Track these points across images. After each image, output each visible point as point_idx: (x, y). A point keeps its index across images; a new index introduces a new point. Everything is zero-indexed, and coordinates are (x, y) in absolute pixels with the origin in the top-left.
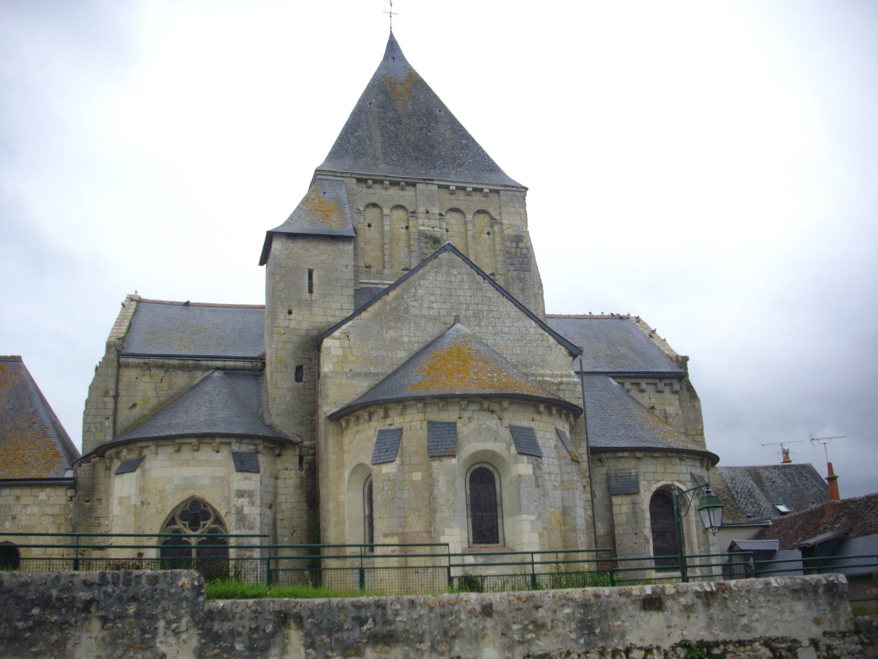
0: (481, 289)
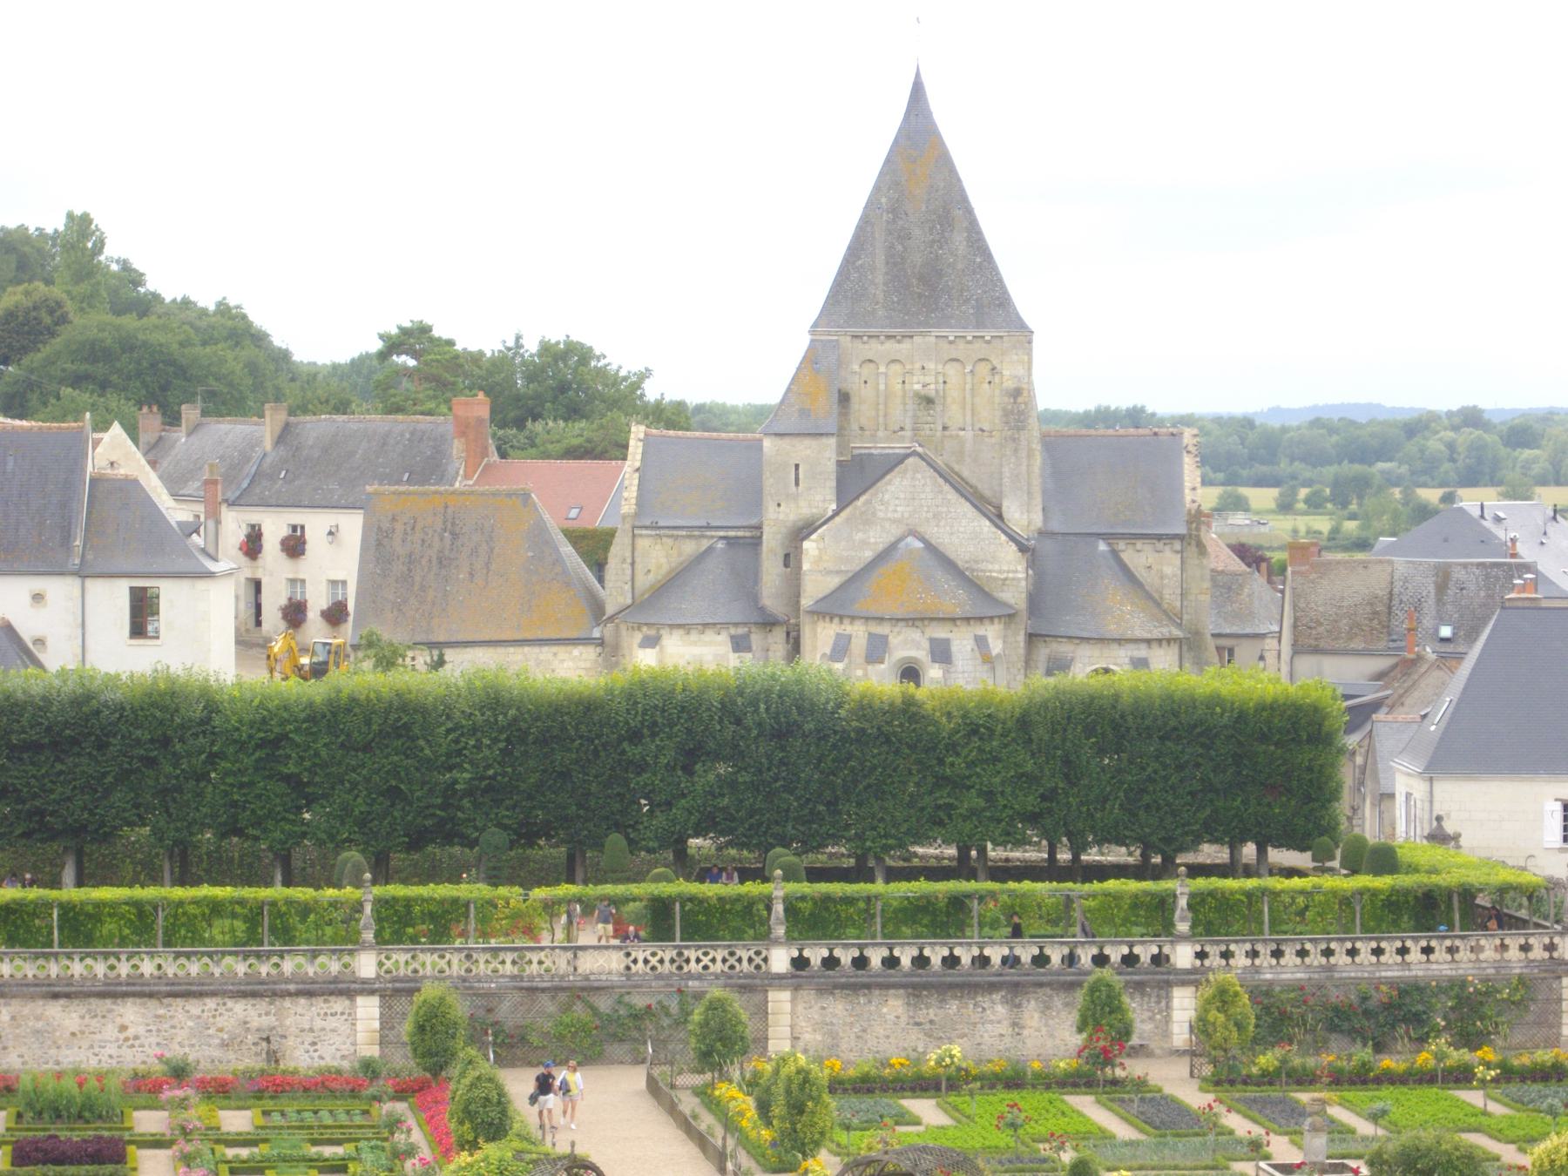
0: (941, 492)
